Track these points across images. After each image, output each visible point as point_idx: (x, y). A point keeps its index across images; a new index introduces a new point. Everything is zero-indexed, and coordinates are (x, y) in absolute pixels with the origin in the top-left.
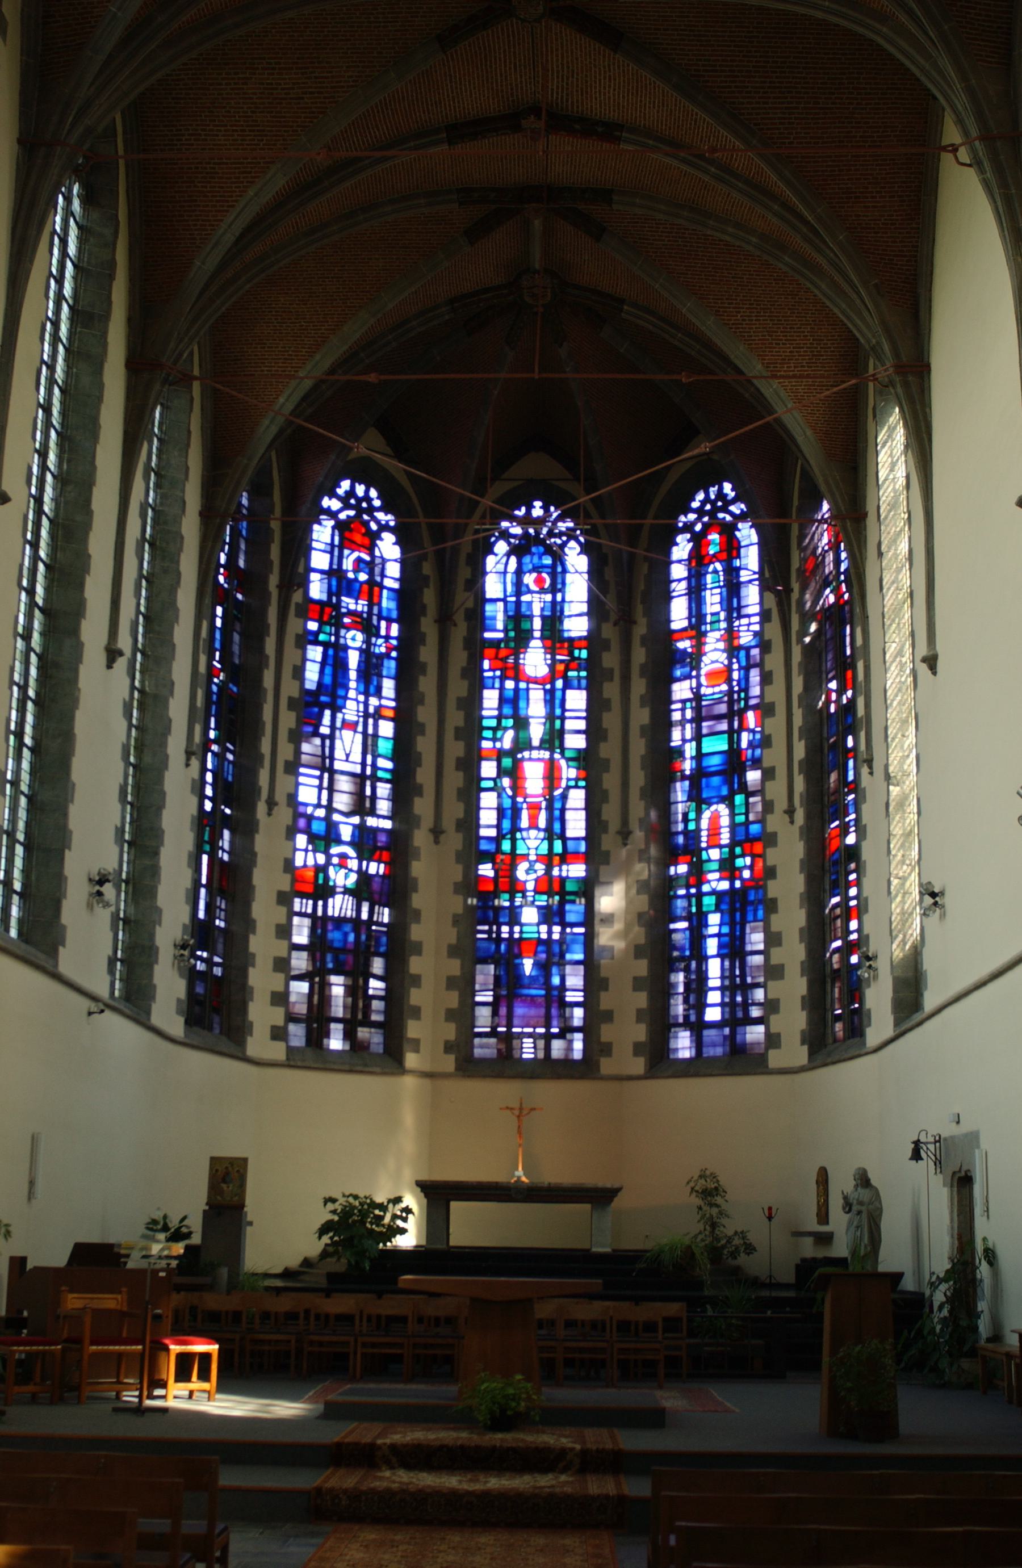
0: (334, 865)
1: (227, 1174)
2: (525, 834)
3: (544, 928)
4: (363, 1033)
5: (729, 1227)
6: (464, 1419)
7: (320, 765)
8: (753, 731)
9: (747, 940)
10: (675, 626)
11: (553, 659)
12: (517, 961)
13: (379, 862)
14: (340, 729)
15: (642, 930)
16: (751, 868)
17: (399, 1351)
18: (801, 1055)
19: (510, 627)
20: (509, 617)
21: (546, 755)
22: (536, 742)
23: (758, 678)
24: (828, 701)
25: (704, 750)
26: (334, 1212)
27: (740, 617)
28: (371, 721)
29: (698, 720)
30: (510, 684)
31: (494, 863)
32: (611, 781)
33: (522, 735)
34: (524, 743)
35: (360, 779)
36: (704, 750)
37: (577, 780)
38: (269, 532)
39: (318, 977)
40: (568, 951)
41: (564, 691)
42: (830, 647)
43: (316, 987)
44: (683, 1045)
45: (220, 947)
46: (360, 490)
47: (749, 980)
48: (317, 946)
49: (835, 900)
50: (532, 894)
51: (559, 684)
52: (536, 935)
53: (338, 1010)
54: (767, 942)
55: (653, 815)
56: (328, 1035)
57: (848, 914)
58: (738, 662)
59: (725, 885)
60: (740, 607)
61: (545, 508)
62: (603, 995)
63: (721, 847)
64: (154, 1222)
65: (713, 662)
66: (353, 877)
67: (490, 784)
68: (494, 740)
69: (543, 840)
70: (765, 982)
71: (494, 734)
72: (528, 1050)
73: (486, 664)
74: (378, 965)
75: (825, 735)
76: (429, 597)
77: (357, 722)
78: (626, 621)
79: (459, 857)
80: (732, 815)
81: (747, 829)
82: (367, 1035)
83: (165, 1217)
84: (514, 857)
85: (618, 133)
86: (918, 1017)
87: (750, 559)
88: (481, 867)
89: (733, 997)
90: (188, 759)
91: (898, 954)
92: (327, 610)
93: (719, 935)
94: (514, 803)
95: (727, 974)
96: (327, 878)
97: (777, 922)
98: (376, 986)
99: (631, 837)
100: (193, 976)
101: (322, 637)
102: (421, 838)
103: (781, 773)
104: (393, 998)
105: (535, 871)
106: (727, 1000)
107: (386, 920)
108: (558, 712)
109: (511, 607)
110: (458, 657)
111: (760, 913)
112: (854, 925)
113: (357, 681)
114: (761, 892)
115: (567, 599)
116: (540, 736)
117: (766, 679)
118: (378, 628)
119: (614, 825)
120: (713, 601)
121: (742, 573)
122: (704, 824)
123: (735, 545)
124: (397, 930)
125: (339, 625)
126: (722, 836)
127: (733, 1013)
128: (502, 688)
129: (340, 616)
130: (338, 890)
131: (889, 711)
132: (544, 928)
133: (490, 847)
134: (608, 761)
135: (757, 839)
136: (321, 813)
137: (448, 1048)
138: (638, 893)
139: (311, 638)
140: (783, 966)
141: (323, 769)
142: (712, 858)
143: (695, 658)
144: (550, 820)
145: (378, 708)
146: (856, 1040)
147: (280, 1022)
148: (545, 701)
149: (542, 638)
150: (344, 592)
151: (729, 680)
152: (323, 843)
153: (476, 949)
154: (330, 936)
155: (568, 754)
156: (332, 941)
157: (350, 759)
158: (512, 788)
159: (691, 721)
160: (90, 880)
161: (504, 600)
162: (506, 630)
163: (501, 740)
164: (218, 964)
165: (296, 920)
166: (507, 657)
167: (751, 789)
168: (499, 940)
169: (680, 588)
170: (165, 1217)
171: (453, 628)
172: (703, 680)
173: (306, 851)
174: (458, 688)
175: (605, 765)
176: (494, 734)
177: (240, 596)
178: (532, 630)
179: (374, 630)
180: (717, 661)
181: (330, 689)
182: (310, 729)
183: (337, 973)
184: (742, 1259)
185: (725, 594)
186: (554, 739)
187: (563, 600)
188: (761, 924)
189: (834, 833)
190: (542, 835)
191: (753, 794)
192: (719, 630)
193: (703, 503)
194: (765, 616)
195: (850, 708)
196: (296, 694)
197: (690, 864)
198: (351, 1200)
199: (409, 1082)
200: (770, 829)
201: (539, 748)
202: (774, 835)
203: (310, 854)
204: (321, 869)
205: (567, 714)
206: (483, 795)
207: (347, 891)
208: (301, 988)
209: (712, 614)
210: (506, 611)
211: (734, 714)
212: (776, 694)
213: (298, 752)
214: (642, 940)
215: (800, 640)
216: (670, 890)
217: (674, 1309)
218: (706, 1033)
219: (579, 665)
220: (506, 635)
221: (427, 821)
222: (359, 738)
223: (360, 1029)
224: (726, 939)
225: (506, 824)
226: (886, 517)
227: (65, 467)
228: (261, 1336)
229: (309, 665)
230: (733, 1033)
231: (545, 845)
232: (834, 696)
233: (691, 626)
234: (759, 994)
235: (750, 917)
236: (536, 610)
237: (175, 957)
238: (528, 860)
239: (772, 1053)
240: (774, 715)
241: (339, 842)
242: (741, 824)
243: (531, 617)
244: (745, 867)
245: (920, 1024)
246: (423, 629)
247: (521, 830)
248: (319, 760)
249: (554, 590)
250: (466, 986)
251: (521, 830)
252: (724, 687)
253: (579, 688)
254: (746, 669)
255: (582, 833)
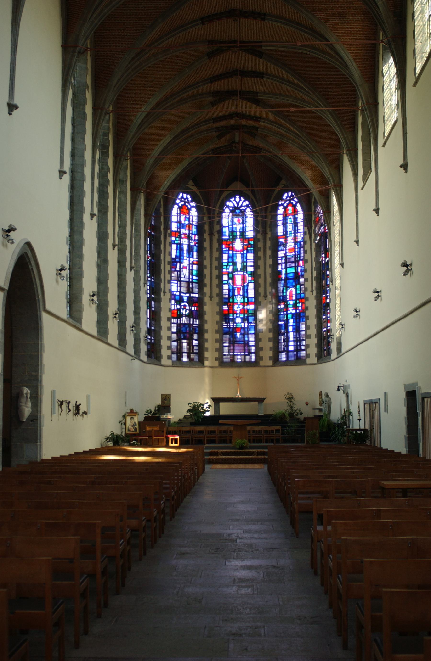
0: (182, 308)
1: (166, 398)
2: (236, 297)
3: (243, 324)
4: (192, 356)
5: (295, 408)
6: (234, 448)
7: (177, 280)
8: (302, 267)
9: (301, 327)
10: (279, 234)
11: (243, 244)
12: (235, 334)
13: (195, 306)
14: (182, 269)
15: (271, 324)
16: (302, 306)
17: (215, 438)
18: (315, 360)
19: (230, 235)
20: (230, 232)
21: (242, 273)
22: (239, 270)
23: (303, 251)
24: (322, 260)
25: (288, 272)
26: (191, 406)
27: (298, 233)
28: (191, 265)
29: (286, 263)
30: (231, 252)
31: (228, 305)
32: (261, 281)
33: (235, 267)
34: (235, 270)
35: (188, 283)
36: (288, 272)
37: (251, 280)
38: (160, 213)
39: (179, 341)
40: (250, 330)
41: (247, 254)
42: (323, 244)
43: (179, 343)
44: (283, 357)
45: (153, 334)
46: (185, 196)
47: (301, 338)
48: (178, 332)
49: (324, 317)
50: (239, 314)
51: (245, 252)
52: (240, 326)
53: (185, 350)
54: (306, 328)
55: (274, 291)
56: (182, 357)
57: (328, 321)
58: (297, 246)
59: (294, 311)
60: (298, 230)
61: (240, 198)
62: (260, 343)
63: (293, 300)
64: (148, 411)
65: (290, 246)
66: (188, 312)
67: (226, 282)
68: (227, 269)
69: (242, 298)
70: (306, 339)
71: (227, 267)
72: (239, 359)
73: (224, 246)
74: (195, 336)
75: (322, 270)
76: (206, 227)
77: (187, 266)
78: (265, 233)
79: (218, 304)
80: (296, 291)
81: (300, 296)
82: (193, 356)
83: (150, 409)
84: (233, 304)
85: (259, 120)
86: (341, 354)
87: (300, 216)
88: (224, 307)
89: (297, 343)
90: (144, 285)
91: (338, 335)
92: (177, 233)
93: (293, 326)
94: (233, 288)
95: (295, 337)
96: (180, 312)
97: (308, 322)
98: (195, 342)
99: (267, 297)
100: (149, 344)
101: (176, 242)
102: (206, 299)
103: (310, 280)
104: (200, 346)
105: (240, 307)
106: (295, 344)
107: (197, 323)
108: (245, 260)
109: (231, 229)
110: (216, 245)
111: (304, 319)
112: (329, 325)
113: (187, 254)
114: (304, 314)
115: (247, 226)
116: (240, 267)
117: (305, 252)
118: (192, 237)
119: (262, 294)
120: (290, 228)
121: (298, 219)
122: (288, 293)
123: (296, 211)
124: (201, 326)
125: (180, 238)
126: (293, 297)
127: (297, 348)
128: (228, 253)
129: (181, 235)
130: (184, 315)
131: (336, 269)
132: (243, 324)
133: (227, 301)
134: (260, 275)
135: (303, 298)
136: (178, 294)
137: (216, 359)
138: (270, 313)
139: (173, 242)
140: (310, 335)
141: (178, 281)
142: (291, 303)
143: (285, 245)
144: (244, 292)
145: (193, 262)
146: (329, 356)
147: (170, 354)
148: (241, 257)
149: (240, 238)
150: (182, 227)
151: (295, 252)
152: (179, 302)
153: (223, 330)
154: (182, 329)
155: (248, 273)
156: (182, 331)
157: (186, 277)
158: (232, 283)
159: (284, 263)
160: (130, 327)
161: (228, 227)
162: (229, 236)
163: (228, 269)
164: (153, 339)
165: (172, 325)
166: (230, 244)
167: (301, 284)
168: (230, 328)
169: (280, 223)
170: (150, 409)
171: (214, 236)
172: (287, 251)
173: (174, 305)
174: (216, 254)
175: (259, 276)
176: (227, 267)
177: (153, 233)
178: (237, 236)
179: (191, 238)
180: (291, 246)
181: (179, 257)
182: (174, 269)
183: (184, 339)
184: (299, 416)
185: (293, 225)
186: (244, 268)
187: (246, 226)
188: (304, 323)
189: (324, 298)
190: (241, 297)
191: (302, 285)
192: (292, 236)
193: (287, 197)
194: (305, 233)
195: (327, 263)
196: (170, 260)
197: (284, 305)
198: (195, 403)
199: (207, 370)
200: (306, 296)
201: (240, 271)
202: (308, 298)
203: (175, 306)
204: (179, 310)
205: (248, 261)
206: (224, 285)
207: (186, 316)
208: (175, 344)
209: (290, 231)
210: (229, 230)
211: (296, 261)
212: (308, 257)
213: (171, 277)
214: (271, 327)
215: (314, 242)
216: (279, 312)
217: (278, 427)
218: (289, 353)
219: (251, 246)
220: (229, 237)
221: (208, 294)
222: (188, 271)
223: (191, 355)
224: (295, 327)
225: (231, 294)
226: (335, 215)
227: (120, 223)
228: (183, 436)
229: (173, 250)
230: (297, 353)
231: (242, 299)
232: (324, 259)
233: (283, 235)
234: (304, 343)
235: (301, 321)
236: (238, 230)
237: (144, 340)
238: (237, 304)
239: (307, 359)
240: (307, 263)
241: (184, 302)
242: (299, 294)
243: (236, 232)
244: (300, 306)
245: (341, 356)
246: (205, 237)
247: (235, 296)
248: (177, 278)
249: (243, 223)
250: (221, 341)
251: (235, 296)
252: (293, 253)
253: (251, 253)
254: (300, 248)
255: (253, 296)
